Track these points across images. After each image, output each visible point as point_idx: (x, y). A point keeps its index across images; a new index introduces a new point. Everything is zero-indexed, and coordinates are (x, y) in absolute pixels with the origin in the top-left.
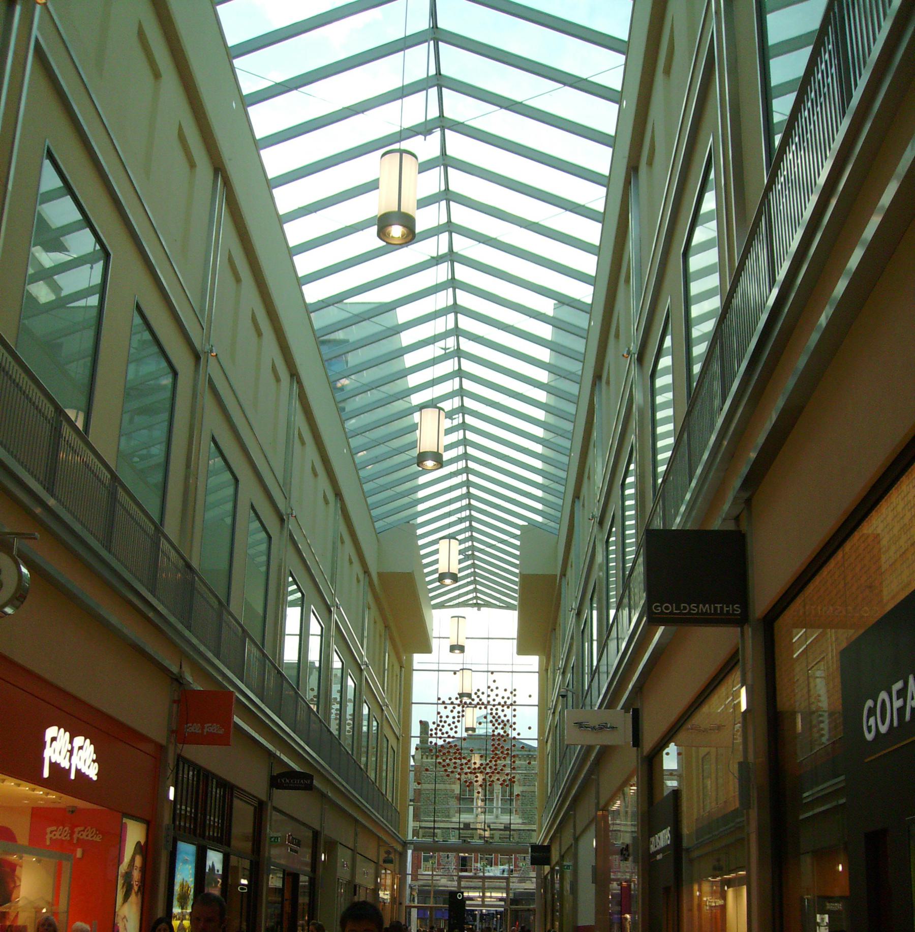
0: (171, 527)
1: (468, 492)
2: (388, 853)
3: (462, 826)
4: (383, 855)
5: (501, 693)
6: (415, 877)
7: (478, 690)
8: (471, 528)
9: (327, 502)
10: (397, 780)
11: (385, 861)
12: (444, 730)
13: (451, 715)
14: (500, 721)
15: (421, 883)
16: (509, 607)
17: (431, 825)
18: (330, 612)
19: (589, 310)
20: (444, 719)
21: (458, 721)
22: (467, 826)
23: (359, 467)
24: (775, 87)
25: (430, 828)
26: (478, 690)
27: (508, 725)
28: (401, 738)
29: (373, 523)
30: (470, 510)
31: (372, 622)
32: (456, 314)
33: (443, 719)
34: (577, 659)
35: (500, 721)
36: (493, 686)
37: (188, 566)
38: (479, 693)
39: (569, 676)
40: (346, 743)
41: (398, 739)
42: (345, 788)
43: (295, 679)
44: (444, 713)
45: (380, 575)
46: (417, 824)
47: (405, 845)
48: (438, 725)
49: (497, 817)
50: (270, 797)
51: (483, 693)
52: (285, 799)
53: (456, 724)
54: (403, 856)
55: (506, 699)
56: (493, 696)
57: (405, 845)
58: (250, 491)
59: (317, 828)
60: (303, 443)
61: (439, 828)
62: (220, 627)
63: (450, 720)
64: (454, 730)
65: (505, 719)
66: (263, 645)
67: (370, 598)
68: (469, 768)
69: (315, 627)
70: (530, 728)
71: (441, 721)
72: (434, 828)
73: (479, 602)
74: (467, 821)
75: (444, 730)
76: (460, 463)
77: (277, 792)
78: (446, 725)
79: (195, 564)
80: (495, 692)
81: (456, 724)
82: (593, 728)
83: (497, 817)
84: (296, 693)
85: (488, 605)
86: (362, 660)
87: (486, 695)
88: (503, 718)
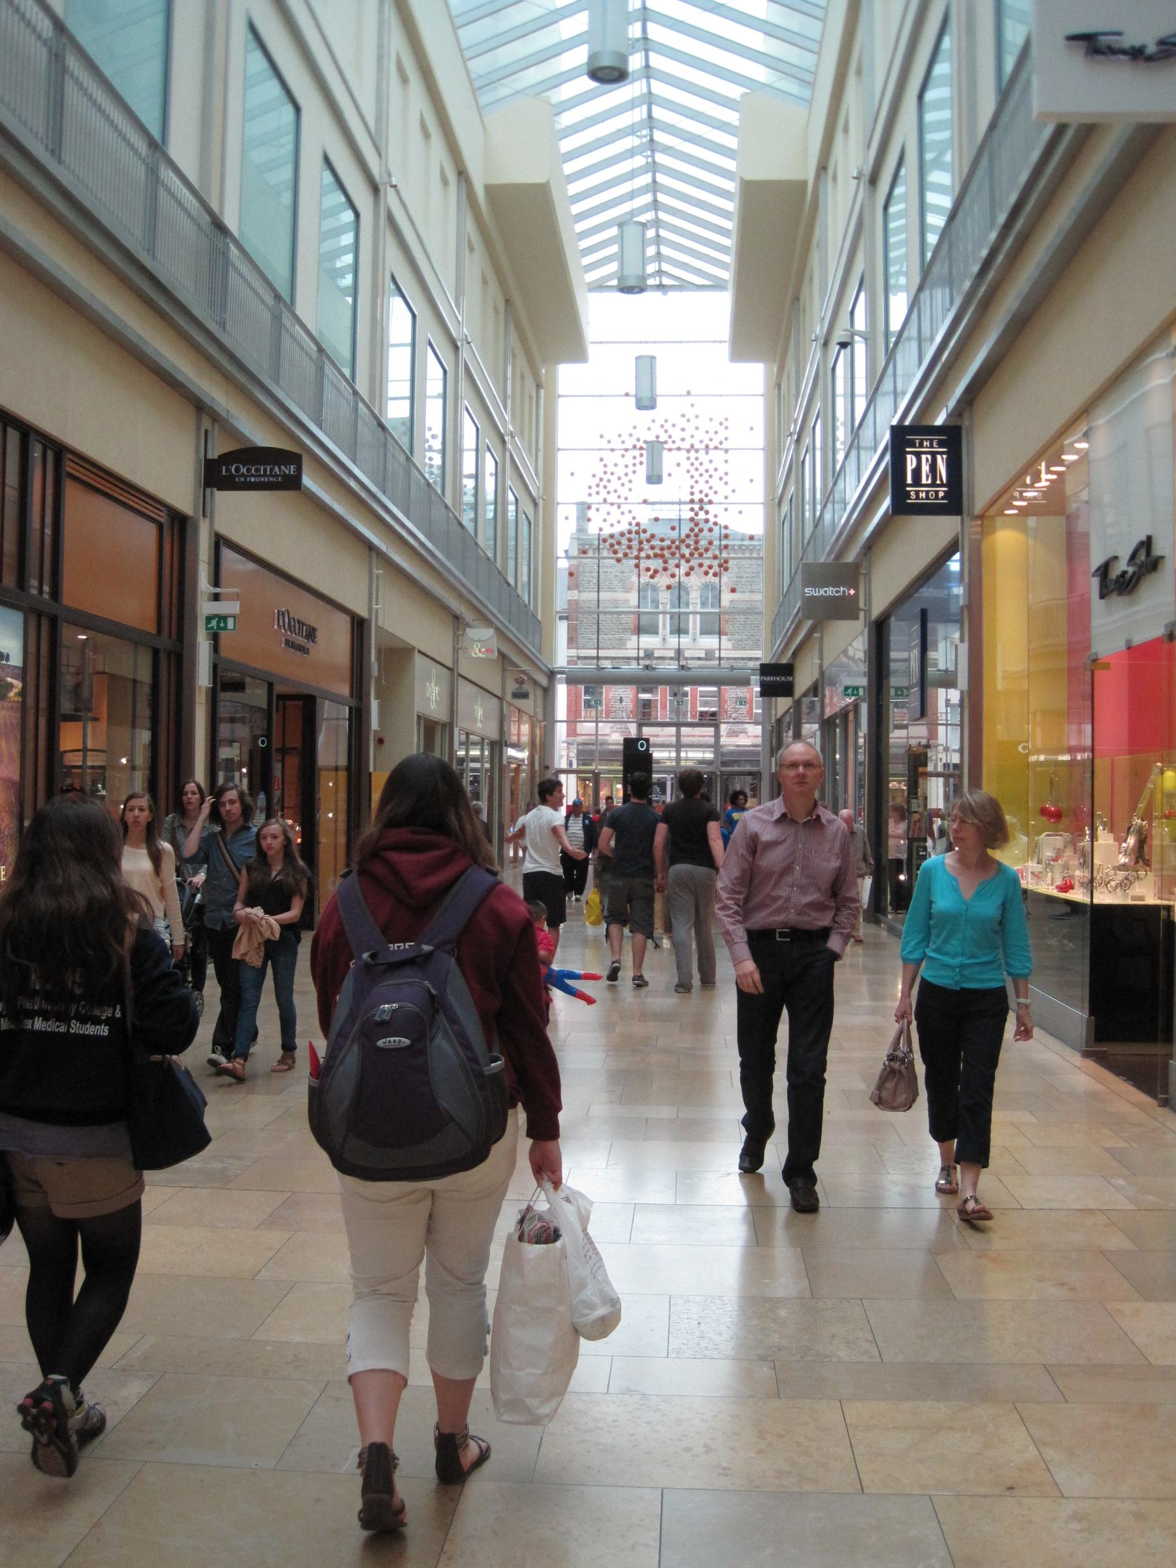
0: (183, 148)
1: (655, 201)
2: (520, 682)
3: (642, 654)
4: (512, 686)
5: (704, 424)
6: (572, 732)
7: (666, 421)
8: (655, 186)
9: (445, 182)
10: (536, 570)
11: (516, 695)
12: (611, 487)
13: (622, 463)
14: (702, 470)
15: (580, 739)
16: (718, 285)
17: (593, 653)
18: (504, 442)
19: (815, 47)
20: (609, 469)
21: (634, 472)
22: (649, 655)
23: (458, 22)
24: (932, 123)
25: (593, 658)
26: (666, 421)
27: (716, 475)
28: (541, 502)
29: (465, 61)
30: (656, 210)
31: (518, 375)
32: (647, 51)
33: (609, 470)
34: (797, 489)
35: (702, 470)
36: (690, 414)
37: (219, 226)
38: (668, 426)
39: (785, 508)
40: (484, 539)
41: (536, 504)
42: (515, 636)
43: (408, 444)
44: (610, 458)
45: (488, 189)
46: (573, 652)
47: (552, 675)
48: (601, 480)
49: (694, 640)
50: (206, 509)
51: (674, 425)
52: (243, 515)
53: (631, 476)
54: (548, 693)
55: (711, 435)
56: (690, 430)
57: (552, 675)
58: (319, 132)
59: (362, 612)
60: (404, 80)
61: (606, 658)
62: (356, 423)
63: (620, 471)
64: (628, 485)
65: (711, 467)
66: (412, 453)
67: (470, 227)
68: (652, 548)
69: (434, 371)
70: (752, 481)
71: (605, 473)
72: (598, 658)
73: (666, 281)
74: (648, 646)
75: (611, 487)
76: (637, 110)
77: (224, 500)
78: (614, 478)
79: (230, 221)
80: (694, 423)
81: (631, 476)
82: (1136, 54)
83: (694, 640)
84: (408, 459)
85: (684, 285)
86: (505, 427)
87: (678, 428)
88: (706, 465)
